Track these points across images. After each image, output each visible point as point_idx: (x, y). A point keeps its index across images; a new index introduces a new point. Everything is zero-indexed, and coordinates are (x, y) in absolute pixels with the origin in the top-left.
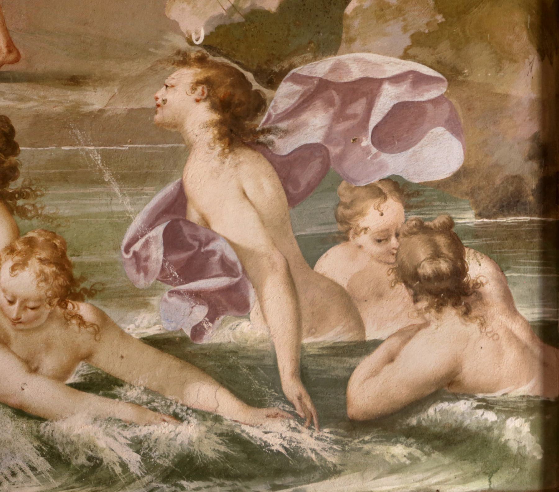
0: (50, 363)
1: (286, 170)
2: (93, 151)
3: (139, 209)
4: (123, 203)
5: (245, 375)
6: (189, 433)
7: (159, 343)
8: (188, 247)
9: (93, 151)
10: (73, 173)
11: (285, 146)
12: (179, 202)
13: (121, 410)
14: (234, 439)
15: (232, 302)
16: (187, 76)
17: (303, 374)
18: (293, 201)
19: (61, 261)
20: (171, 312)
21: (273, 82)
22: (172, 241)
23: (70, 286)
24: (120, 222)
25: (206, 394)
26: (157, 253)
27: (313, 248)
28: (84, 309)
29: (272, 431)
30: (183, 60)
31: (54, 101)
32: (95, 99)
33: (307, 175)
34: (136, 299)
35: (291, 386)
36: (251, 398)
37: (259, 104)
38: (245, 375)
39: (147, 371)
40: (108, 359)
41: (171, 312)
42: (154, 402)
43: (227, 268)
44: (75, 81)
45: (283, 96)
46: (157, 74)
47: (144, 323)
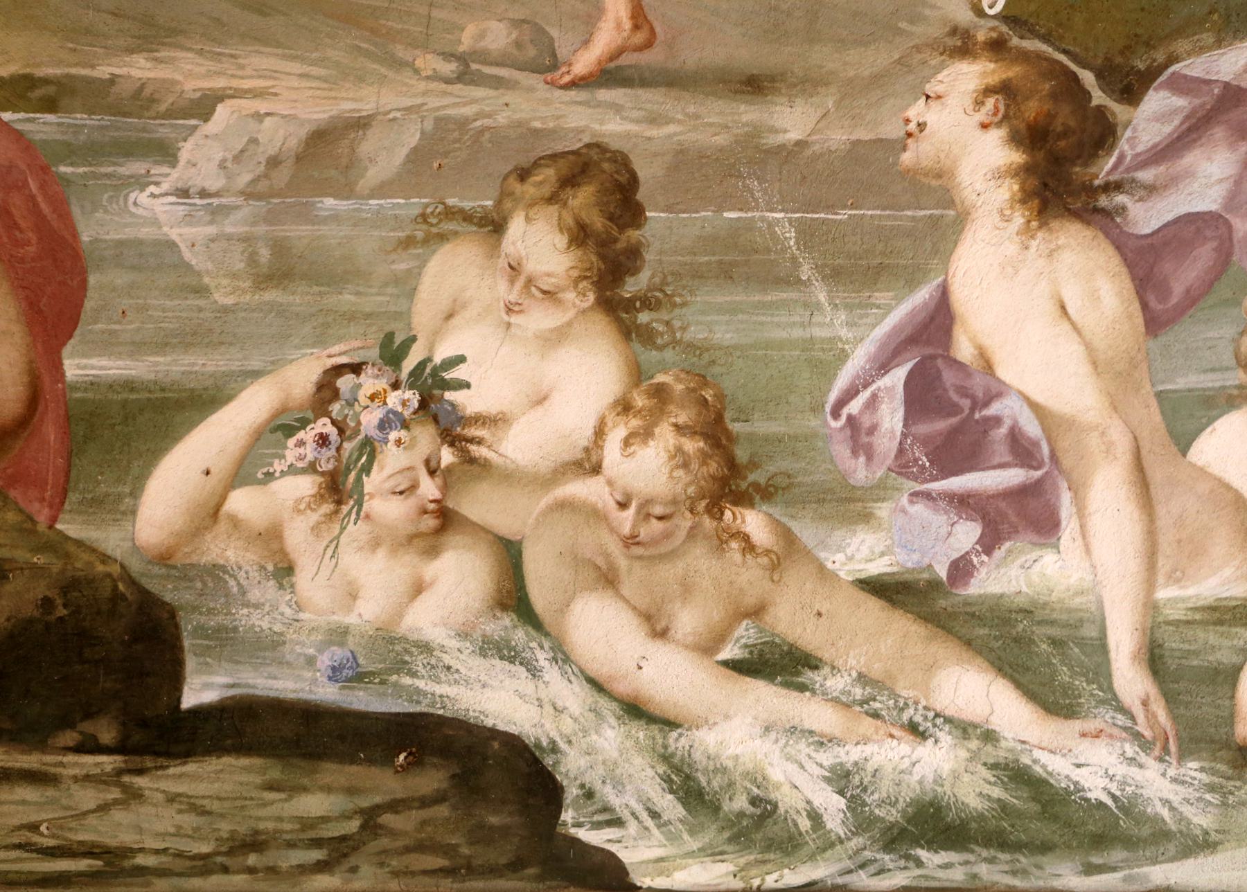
0: (688, 620)
1: (1145, 263)
2: (782, 223)
3: (860, 335)
4: (832, 323)
5: (1042, 655)
6: (936, 765)
7: (888, 590)
8: (951, 410)
9: (782, 223)
10: (743, 264)
11: (1146, 217)
12: (938, 322)
13: (815, 713)
14: (1017, 775)
15: (1027, 515)
16: (966, 78)
17: (1154, 659)
18: (1154, 324)
19: (714, 430)
20: (912, 533)
21: (1131, 89)
22: (922, 397)
23: (729, 477)
24: (826, 359)
25: (971, 688)
26: (891, 418)
27: (1186, 417)
28: (754, 522)
29: (1089, 763)
30: (961, 45)
31: (713, 122)
32: (791, 121)
33: (1184, 275)
34: (848, 506)
35: (1130, 680)
36: (1056, 703)
37: (1103, 134)
38: (1042, 655)
39: (868, 641)
40: (792, 620)
41: (912, 533)
42: (874, 701)
43: (1022, 450)
44: (754, 85)
45: (1151, 118)
46: (909, 76)
47: (862, 552)
